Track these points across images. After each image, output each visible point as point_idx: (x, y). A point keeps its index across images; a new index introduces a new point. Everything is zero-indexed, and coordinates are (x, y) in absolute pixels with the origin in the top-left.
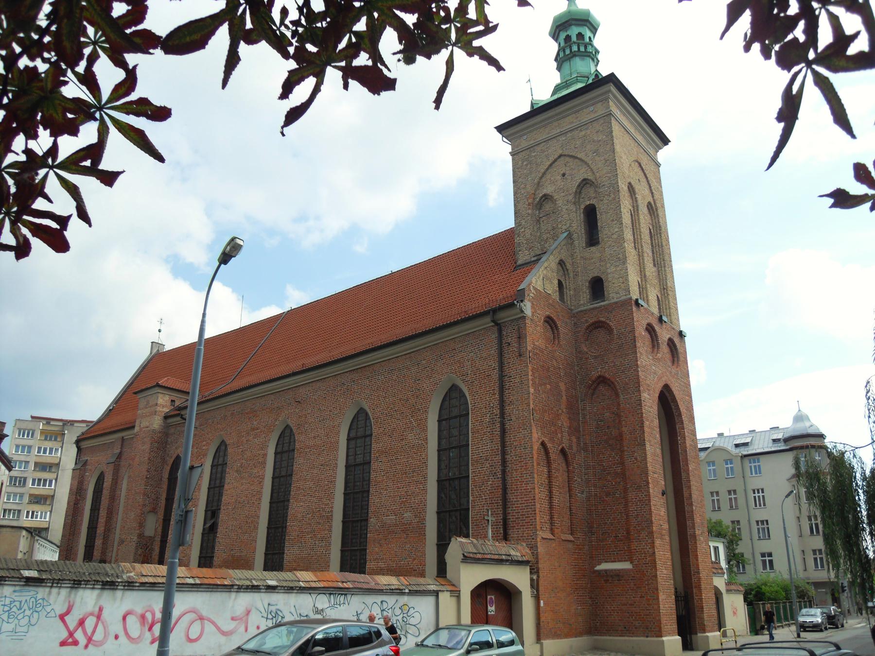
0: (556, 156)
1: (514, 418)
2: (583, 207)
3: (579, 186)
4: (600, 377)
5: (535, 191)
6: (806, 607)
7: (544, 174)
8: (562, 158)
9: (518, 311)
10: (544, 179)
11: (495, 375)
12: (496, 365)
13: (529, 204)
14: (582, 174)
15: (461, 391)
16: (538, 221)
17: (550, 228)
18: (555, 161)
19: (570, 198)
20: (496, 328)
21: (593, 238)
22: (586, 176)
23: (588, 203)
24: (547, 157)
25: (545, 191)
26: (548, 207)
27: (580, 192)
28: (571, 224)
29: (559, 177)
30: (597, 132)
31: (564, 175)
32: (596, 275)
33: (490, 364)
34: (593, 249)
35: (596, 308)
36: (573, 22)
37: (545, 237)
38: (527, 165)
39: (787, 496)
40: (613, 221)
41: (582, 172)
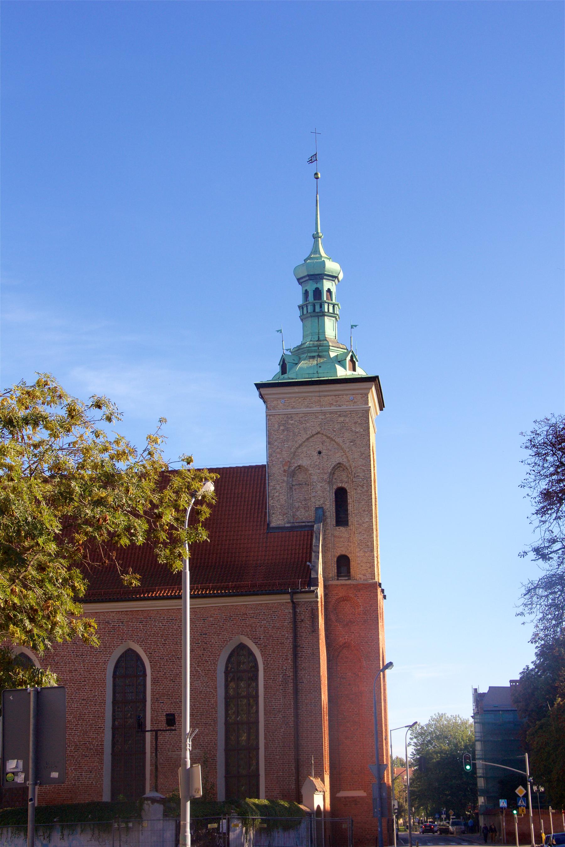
0: (314, 433)
1: (305, 681)
2: (335, 487)
3: (334, 468)
4: (345, 643)
5: (292, 459)
6: (263, 821)
7: (301, 445)
8: (319, 435)
9: (314, 596)
10: (300, 450)
11: (289, 643)
12: (291, 636)
13: (285, 471)
14: (338, 458)
15: (251, 653)
16: (291, 488)
17: (302, 498)
18: (313, 436)
19: (326, 477)
20: (291, 605)
21: (342, 519)
22: (341, 461)
23: (340, 485)
24: (305, 429)
25: (300, 463)
26: (301, 477)
27: (334, 473)
28: (324, 501)
29: (316, 454)
30: (355, 423)
31: (320, 453)
32: (343, 553)
33: (283, 634)
34: (342, 529)
35: (346, 585)
36: (325, 277)
37: (297, 505)
38: (283, 431)
39: (406, 727)
40: (364, 511)
41: (337, 455)
